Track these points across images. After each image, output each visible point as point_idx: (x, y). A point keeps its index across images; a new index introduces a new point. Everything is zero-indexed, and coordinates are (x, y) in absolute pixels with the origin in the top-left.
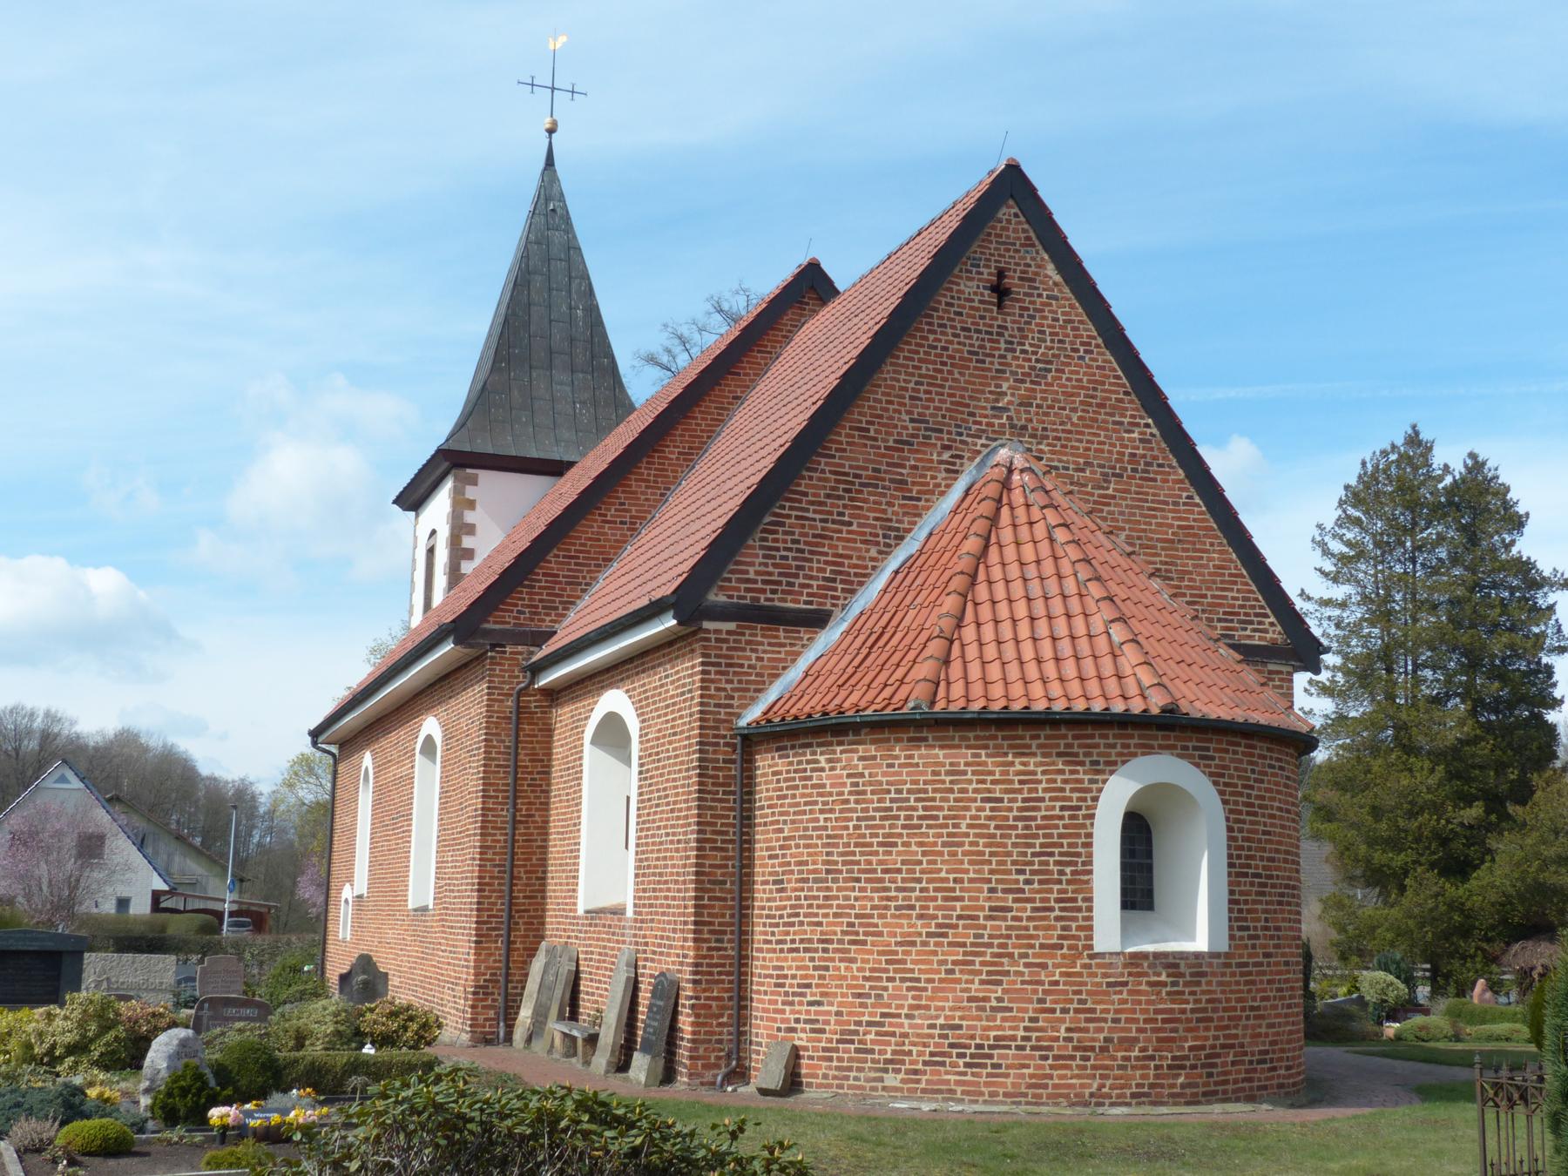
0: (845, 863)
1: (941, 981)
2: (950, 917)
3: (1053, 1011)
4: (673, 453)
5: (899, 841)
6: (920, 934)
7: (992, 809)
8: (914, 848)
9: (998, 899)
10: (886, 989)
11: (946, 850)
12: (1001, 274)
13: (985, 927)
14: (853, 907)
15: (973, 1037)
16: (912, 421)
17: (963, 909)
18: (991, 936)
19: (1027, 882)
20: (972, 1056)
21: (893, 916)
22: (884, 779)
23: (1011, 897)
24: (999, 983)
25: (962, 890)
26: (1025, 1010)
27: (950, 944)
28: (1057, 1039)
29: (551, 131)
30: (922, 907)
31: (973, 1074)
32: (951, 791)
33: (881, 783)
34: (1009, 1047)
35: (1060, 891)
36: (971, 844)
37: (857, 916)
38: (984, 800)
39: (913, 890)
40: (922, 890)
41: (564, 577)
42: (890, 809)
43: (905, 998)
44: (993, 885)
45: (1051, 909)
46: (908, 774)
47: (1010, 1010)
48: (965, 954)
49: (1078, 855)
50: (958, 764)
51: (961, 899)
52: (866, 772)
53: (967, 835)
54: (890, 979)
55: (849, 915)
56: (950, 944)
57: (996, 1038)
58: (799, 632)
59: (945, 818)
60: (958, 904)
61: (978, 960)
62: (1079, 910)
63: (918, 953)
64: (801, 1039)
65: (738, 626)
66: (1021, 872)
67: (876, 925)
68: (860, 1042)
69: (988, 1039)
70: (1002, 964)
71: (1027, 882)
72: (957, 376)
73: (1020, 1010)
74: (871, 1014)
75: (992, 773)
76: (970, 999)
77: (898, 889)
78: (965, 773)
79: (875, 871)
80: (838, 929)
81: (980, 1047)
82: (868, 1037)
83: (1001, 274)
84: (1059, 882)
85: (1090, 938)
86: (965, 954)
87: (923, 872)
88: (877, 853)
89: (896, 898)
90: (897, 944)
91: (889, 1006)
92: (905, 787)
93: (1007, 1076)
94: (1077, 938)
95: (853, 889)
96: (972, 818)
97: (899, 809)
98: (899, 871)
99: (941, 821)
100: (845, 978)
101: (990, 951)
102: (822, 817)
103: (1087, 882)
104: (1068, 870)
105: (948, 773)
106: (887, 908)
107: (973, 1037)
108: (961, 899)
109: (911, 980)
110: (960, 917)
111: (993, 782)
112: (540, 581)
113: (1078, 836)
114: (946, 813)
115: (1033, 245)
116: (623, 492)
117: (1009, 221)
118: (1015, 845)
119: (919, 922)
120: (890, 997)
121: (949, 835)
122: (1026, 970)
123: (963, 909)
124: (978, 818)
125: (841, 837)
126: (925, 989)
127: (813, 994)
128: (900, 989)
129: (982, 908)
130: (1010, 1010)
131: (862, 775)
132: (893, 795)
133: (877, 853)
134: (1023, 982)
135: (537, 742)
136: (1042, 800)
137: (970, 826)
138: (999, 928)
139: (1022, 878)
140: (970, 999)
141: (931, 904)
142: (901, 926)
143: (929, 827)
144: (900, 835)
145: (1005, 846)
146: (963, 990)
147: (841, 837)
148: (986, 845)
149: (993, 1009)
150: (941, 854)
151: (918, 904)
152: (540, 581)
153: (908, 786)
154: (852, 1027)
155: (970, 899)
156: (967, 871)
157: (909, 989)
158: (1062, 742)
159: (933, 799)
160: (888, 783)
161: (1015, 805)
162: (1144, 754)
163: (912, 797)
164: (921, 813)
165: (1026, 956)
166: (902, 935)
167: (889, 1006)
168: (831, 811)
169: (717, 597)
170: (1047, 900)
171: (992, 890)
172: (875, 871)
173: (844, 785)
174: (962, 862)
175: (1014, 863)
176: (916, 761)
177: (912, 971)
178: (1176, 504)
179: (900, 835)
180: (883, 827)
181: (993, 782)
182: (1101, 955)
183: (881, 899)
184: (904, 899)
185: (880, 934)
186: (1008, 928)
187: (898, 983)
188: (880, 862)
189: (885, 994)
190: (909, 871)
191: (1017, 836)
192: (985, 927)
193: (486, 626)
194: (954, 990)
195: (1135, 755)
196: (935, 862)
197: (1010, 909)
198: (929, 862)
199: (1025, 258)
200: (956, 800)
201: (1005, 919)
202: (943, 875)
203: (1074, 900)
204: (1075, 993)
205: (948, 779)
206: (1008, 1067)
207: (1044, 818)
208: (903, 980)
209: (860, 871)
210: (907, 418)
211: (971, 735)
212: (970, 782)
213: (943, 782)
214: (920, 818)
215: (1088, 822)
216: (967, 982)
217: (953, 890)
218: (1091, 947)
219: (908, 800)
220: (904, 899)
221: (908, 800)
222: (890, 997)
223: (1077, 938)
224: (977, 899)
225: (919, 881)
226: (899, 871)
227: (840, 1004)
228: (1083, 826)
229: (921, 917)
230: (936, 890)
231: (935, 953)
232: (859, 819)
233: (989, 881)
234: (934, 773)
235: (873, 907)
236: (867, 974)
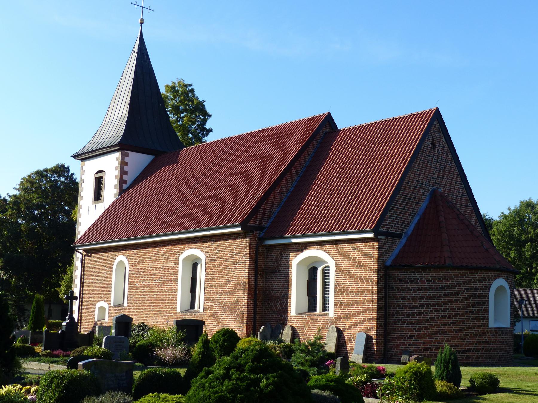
0: (426, 304)
1: (454, 334)
2: (456, 318)
3: (480, 342)
4: (294, 171)
5: (407, 298)
6: (448, 323)
7: (467, 291)
8: (446, 301)
9: (468, 314)
10: (439, 337)
11: (455, 301)
12: (433, 140)
13: (465, 321)
14: (429, 315)
15: (462, 349)
16: (417, 181)
17: (459, 316)
18: (466, 323)
19: (475, 310)
20: (462, 353)
21: (440, 318)
22: (438, 282)
23: (471, 313)
24: (468, 335)
25: (459, 312)
26: (474, 342)
27: (456, 325)
28: (481, 349)
29: (142, 23)
30: (449, 316)
31: (462, 358)
32: (456, 286)
33: (437, 283)
34: (470, 351)
35: (406, 308)
36: (462, 300)
37: (430, 318)
38: (465, 289)
39: (446, 311)
40: (449, 311)
41: (268, 210)
42: (440, 290)
43: (444, 339)
44: (467, 310)
45: (480, 317)
46: (445, 281)
47: (471, 342)
48: (460, 328)
49: (486, 303)
50: (458, 279)
51: (459, 314)
52: (432, 280)
53: (460, 298)
54: (440, 334)
55: (427, 318)
56: (456, 325)
57: (467, 349)
58: (396, 240)
59: (455, 293)
60: (458, 315)
61: (463, 329)
62: (486, 317)
63: (448, 327)
64: (411, 350)
65: (385, 238)
66: (473, 307)
67: (436, 320)
68: (431, 350)
69: (465, 349)
70: (469, 330)
71: (475, 310)
72: (425, 168)
73: (473, 342)
74: (434, 343)
75: (467, 282)
76: (461, 339)
77: (442, 311)
78: (460, 282)
79: (435, 306)
80: (424, 321)
81: (463, 351)
82: (433, 349)
83: (433, 140)
84: (482, 310)
85: (488, 324)
86: (460, 328)
87: (449, 307)
88: (436, 302)
89: (442, 313)
90: (442, 325)
91: (439, 341)
92: (444, 285)
93: (470, 358)
94: (485, 324)
95: (429, 311)
96: (462, 293)
97: (442, 290)
98: (442, 306)
99: (454, 294)
100: (426, 334)
101: (466, 327)
102: (418, 291)
103: (487, 310)
104: (483, 307)
105: (455, 282)
106: (439, 316)
107: (462, 349)
108: (459, 314)
109: (446, 334)
110: (459, 318)
111: (467, 284)
112: (262, 211)
113: (485, 298)
114: (455, 292)
115: (440, 132)
116: (282, 183)
117: (436, 125)
118: (472, 300)
119: (448, 320)
120: (440, 339)
121: (456, 297)
122: (474, 332)
123: (459, 316)
124: (463, 293)
125: (425, 297)
126: (450, 337)
127: (415, 338)
128: (443, 336)
129: (464, 316)
130: (471, 342)
131: (431, 281)
132: (440, 287)
133: (436, 302)
134: (474, 335)
135: (262, 262)
136: (478, 289)
137: (461, 295)
138: (468, 321)
139: (473, 309)
140: (461, 339)
141: (451, 315)
142: (443, 321)
143: (450, 295)
144: (443, 297)
145: (470, 300)
146: (459, 337)
147: (425, 297)
148: (465, 300)
149: (467, 341)
150: (454, 302)
151: (448, 315)
152: (262, 211)
153: (445, 284)
154: (429, 347)
155: (461, 314)
156: (460, 307)
157: (445, 337)
158: (483, 275)
159: (452, 288)
160: (439, 283)
161: (472, 290)
162: (498, 278)
163: (446, 287)
164: (448, 291)
165: (474, 328)
166: (443, 323)
167: (439, 341)
168: (421, 290)
169: (381, 229)
170: (479, 314)
171: (467, 312)
172: (435, 306)
173: (426, 283)
174: (459, 304)
175: (472, 305)
176: (447, 278)
177: (446, 332)
178: (467, 206)
179: (443, 297)
180: (438, 295)
181: (467, 284)
182: (490, 328)
183: (437, 313)
184: (444, 314)
185: (437, 322)
186: (470, 321)
187: (442, 335)
188: (437, 304)
189: (438, 338)
190: (445, 306)
191: (473, 298)
192: (465, 321)
193: (249, 224)
194: (457, 337)
195: (496, 278)
196: (452, 304)
197: (471, 317)
198: (450, 304)
199: (438, 136)
200: (458, 289)
201: (470, 319)
202: (454, 308)
203: (485, 314)
204: (485, 337)
205: (456, 283)
206: (470, 356)
207: (479, 294)
208: (443, 334)
209: (430, 306)
210: (416, 180)
211: (462, 272)
212: (461, 284)
213: (454, 284)
214: (448, 293)
215: (488, 295)
216: (460, 335)
217: (457, 312)
218: (488, 326)
219: (445, 288)
220: (444, 314)
221: (447, 288)
222: (440, 339)
223: (485, 324)
224: (463, 314)
225: (448, 309)
226: (442, 306)
227: (424, 341)
228: (487, 296)
229: (448, 318)
230: (452, 311)
231: (452, 327)
232: (430, 292)
233: (466, 309)
234: (452, 281)
235: (435, 316)
236: (433, 333)
